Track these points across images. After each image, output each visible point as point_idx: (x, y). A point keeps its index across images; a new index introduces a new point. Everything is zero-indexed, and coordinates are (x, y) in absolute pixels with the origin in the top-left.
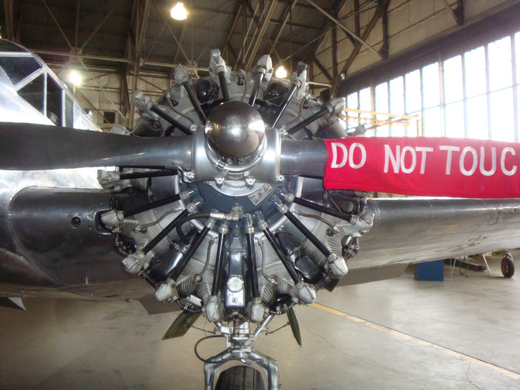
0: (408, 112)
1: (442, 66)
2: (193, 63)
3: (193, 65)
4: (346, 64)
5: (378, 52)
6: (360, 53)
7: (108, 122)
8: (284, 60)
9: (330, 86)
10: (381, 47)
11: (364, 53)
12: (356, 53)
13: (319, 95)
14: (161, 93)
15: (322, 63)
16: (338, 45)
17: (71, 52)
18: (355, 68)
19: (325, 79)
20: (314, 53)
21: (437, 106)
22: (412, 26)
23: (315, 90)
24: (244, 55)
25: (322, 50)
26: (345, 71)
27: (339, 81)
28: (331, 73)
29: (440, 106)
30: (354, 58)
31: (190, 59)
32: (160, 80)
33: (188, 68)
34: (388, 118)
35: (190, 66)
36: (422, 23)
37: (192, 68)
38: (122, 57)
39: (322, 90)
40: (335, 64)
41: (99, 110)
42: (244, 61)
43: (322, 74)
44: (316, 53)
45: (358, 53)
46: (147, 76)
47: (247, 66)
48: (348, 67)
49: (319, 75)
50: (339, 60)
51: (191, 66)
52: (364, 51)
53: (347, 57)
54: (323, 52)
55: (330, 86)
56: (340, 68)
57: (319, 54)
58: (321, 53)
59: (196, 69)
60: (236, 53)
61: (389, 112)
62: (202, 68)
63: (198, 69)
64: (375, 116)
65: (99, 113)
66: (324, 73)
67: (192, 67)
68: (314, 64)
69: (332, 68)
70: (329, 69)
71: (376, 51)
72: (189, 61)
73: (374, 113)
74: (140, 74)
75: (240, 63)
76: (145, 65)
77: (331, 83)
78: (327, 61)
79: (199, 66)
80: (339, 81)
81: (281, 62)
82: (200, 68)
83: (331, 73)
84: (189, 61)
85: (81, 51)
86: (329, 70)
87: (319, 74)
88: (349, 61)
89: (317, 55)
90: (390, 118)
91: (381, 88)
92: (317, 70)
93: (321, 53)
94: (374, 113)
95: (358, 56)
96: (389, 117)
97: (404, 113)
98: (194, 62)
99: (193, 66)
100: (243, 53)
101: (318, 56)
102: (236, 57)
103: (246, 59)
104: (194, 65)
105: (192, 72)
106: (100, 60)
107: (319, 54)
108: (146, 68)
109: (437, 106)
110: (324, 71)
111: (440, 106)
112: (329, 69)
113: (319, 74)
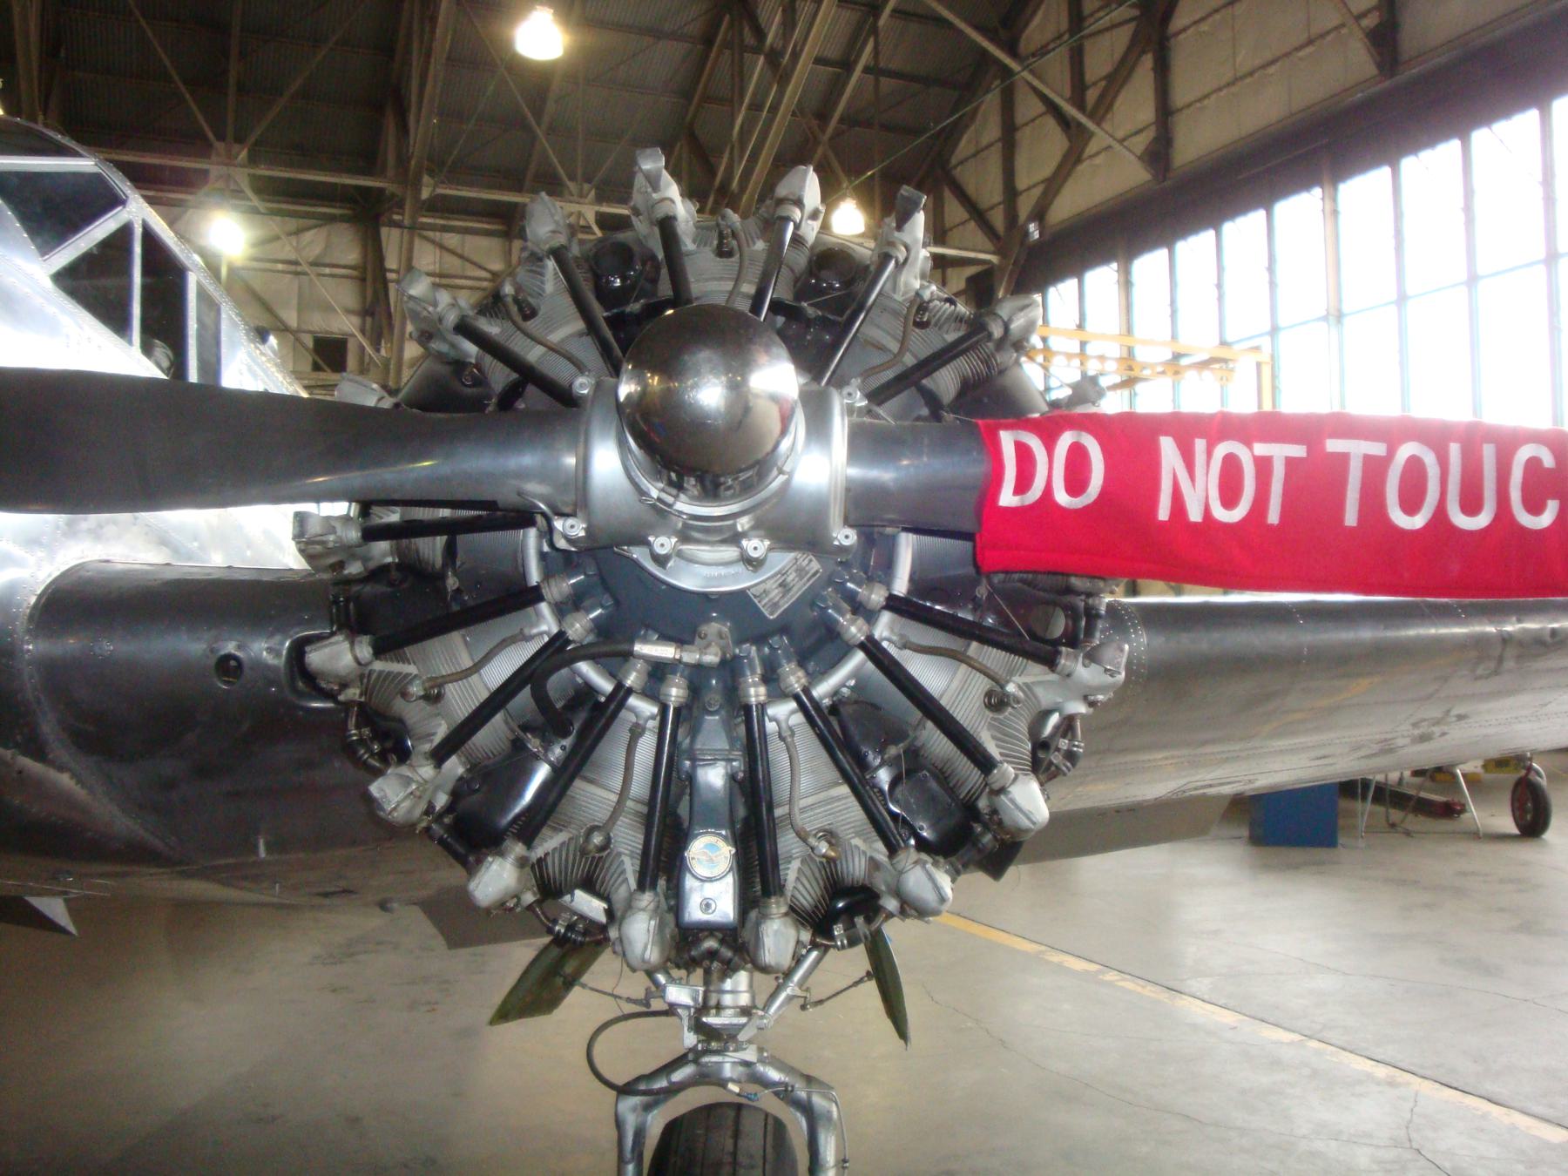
0: (1229, 338)
1: (1334, 200)
2: (581, 189)
3: (582, 195)
4: (1045, 194)
5: (1140, 158)
6: (1087, 159)
7: (325, 367)
8: (857, 182)
9: (994, 259)
10: (1150, 143)
11: (1098, 160)
12: (1072, 159)
13: (962, 285)
14: (485, 280)
15: (971, 189)
16: (1018, 135)
17: (214, 158)
18: (1070, 204)
19: (980, 238)
20: (948, 161)
21: (1319, 319)
22: (1242, 78)
23: (949, 271)
24: (736, 165)
25: (972, 150)
26: (1039, 215)
27: (1022, 243)
28: (998, 219)
29: (1325, 318)
30: (1069, 174)
31: (572, 178)
32: (484, 242)
33: (568, 204)
34: (1169, 356)
35: (571, 198)
36: (1272, 70)
37: (578, 205)
38: (367, 171)
39: (971, 271)
40: (1011, 193)
41: (299, 331)
42: (735, 184)
43: (972, 224)
44: (954, 161)
45: (1079, 161)
46: (445, 229)
47: (745, 198)
48: (1051, 203)
49: (961, 228)
50: (1022, 182)
51: (575, 198)
52: (1098, 153)
53: (1047, 171)
54: (974, 155)
55: (994, 259)
56: (1025, 206)
57: (961, 163)
58: (967, 159)
59: (591, 207)
60: (712, 160)
61: (1174, 337)
62: (610, 206)
63: (597, 208)
64: (1130, 350)
65: (297, 340)
66: (976, 221)
67: (578, 203)
68: (948, 194)
69: (1002, 206)
70: (992, 208)
71: (1134, 154)
72: (571, 185)
73: (1128, 341)
74: (422, 223)
75: (723, 190)
76: (438, 195)
77: (997, 252)
78: (986, 184)
79: (600, 199)
80: (1022, 243)
81: (847, 188)
82: (602, 206)
83: (998, 219)
84: (571, 185)
85: (244, 154)
86: (992, 212)
87: (963, 223)
88: (1053, 185)
89: (955, 167)
90: (1177, 356)
91: (1150, 265)
92: (955, 211)
93: (967, 159)
94: (1128, 341)
95: (1080, 168)
96: (1173, 353)
97: (1217, 342)
98: (586, 186)
99: (582, 200)
100: (731, 159)
101: (959, 169)
102: (711, 171)
103: (741, 176)
104: (586, 197)
105: (579, 218)
106: (301, 181)
107: (961, 163)
108: (439, 206)
109: (1319, 319)
110: (978, 215)
111: (1325, 318)
112: (992, 208)
113: (963, 223)
